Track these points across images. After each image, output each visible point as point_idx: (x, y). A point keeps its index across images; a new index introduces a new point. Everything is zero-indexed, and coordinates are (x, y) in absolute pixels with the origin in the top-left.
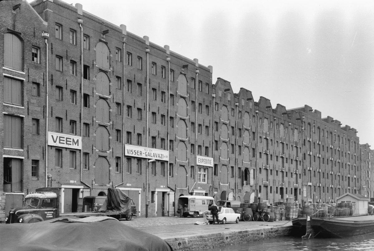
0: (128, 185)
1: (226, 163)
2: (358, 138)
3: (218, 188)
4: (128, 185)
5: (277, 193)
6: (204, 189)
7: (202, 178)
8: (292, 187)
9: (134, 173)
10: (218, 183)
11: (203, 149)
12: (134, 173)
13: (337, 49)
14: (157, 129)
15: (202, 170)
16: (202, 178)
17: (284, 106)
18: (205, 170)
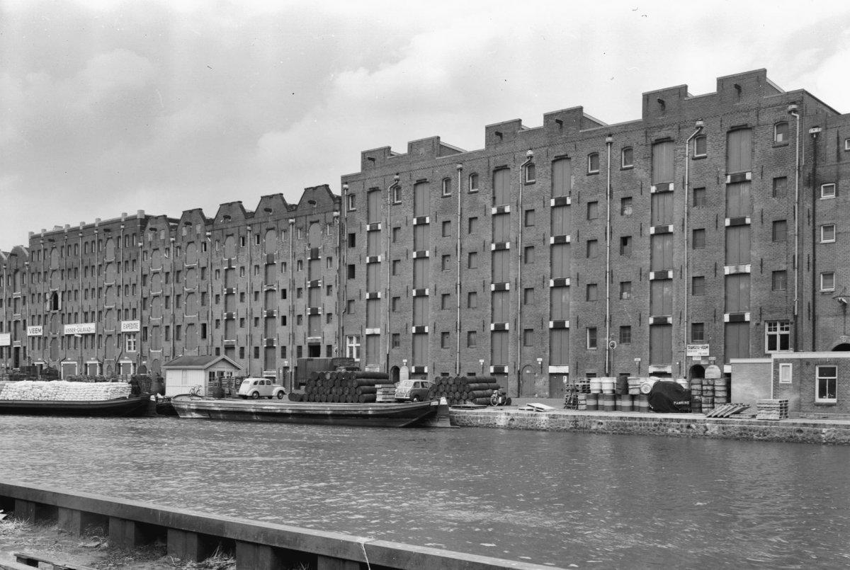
0: (69, 359)
1: (158, 323)
2: (721, 82)
3: (147, 355)
4: (69, 359)
5: (10, 357)
6: (131, 359)
7: (132, 346)
8: (302, 343)
9: (72, 349)
10: (147, 350)
11: (130, 312)
12: (72, 349)
13: (822, 41)
14: (90, 304)
15: (132, 336)
16: (132, 346)
17: (274, 195)
18: (134, 335)
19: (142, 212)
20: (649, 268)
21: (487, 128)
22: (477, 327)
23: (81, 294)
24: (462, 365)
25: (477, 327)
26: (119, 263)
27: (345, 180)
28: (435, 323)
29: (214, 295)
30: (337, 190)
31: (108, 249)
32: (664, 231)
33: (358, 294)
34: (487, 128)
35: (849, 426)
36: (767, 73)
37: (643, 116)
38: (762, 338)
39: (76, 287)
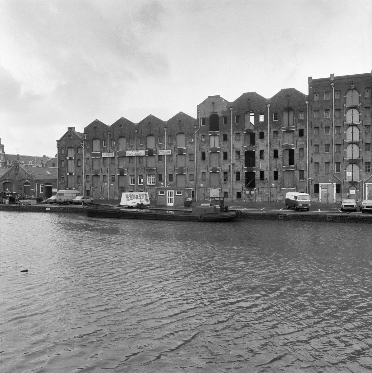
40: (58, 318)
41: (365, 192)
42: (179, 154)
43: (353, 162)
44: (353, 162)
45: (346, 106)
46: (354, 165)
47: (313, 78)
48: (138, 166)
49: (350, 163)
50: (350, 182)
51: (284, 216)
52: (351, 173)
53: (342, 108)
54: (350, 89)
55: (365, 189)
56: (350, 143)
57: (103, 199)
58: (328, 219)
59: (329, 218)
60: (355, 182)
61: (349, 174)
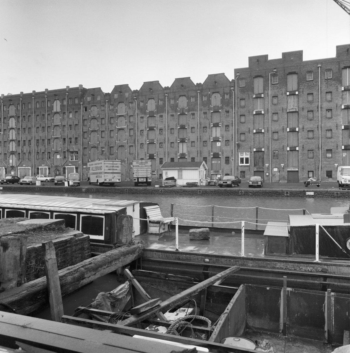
4: (43, 165)
19: (81, 86)
20: (253, 128)
21: (337, 47)
22: (332, 147)
23: (34, 130)
24: (322, 167)
25: (332, 147)
26: (19, 117)
27: (237, 71)
28: (303, 145)
29: (139, 130)
30: (231, 76)
31: (10, 109)
32: (260, 113)
33: (247, 130)
34: (337, 47)
35: (6, 190)
36: (269, 56)
37: (337, 56)
38: (238, 160)
39: (30, 126)
40: (64, 280)
41: (18, 173)
42: (180, 142)
43: (13, 153)
44: (13, 153)
45: (9, 116)
46: (13, 155)
47: (24, 93)
48: (168, 151)
49: (11, 154)
50: (11, 166)
51: (290, 193)
52: (11, 160)
53: (7, 117)
54: (10, 105)
55: (18, 171)
56: (11, 141)
57: (129, 180)
58: (285, 195)
59: (287, 193)
60: (13, 166)
61: (11, 161)
